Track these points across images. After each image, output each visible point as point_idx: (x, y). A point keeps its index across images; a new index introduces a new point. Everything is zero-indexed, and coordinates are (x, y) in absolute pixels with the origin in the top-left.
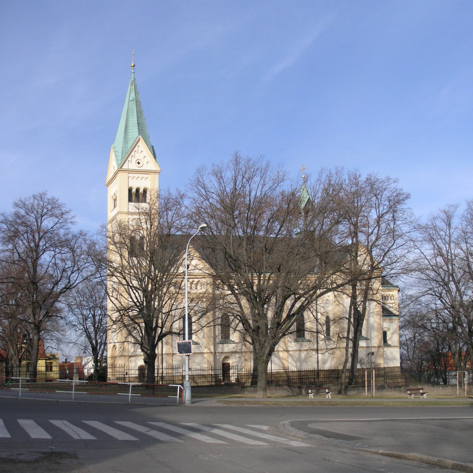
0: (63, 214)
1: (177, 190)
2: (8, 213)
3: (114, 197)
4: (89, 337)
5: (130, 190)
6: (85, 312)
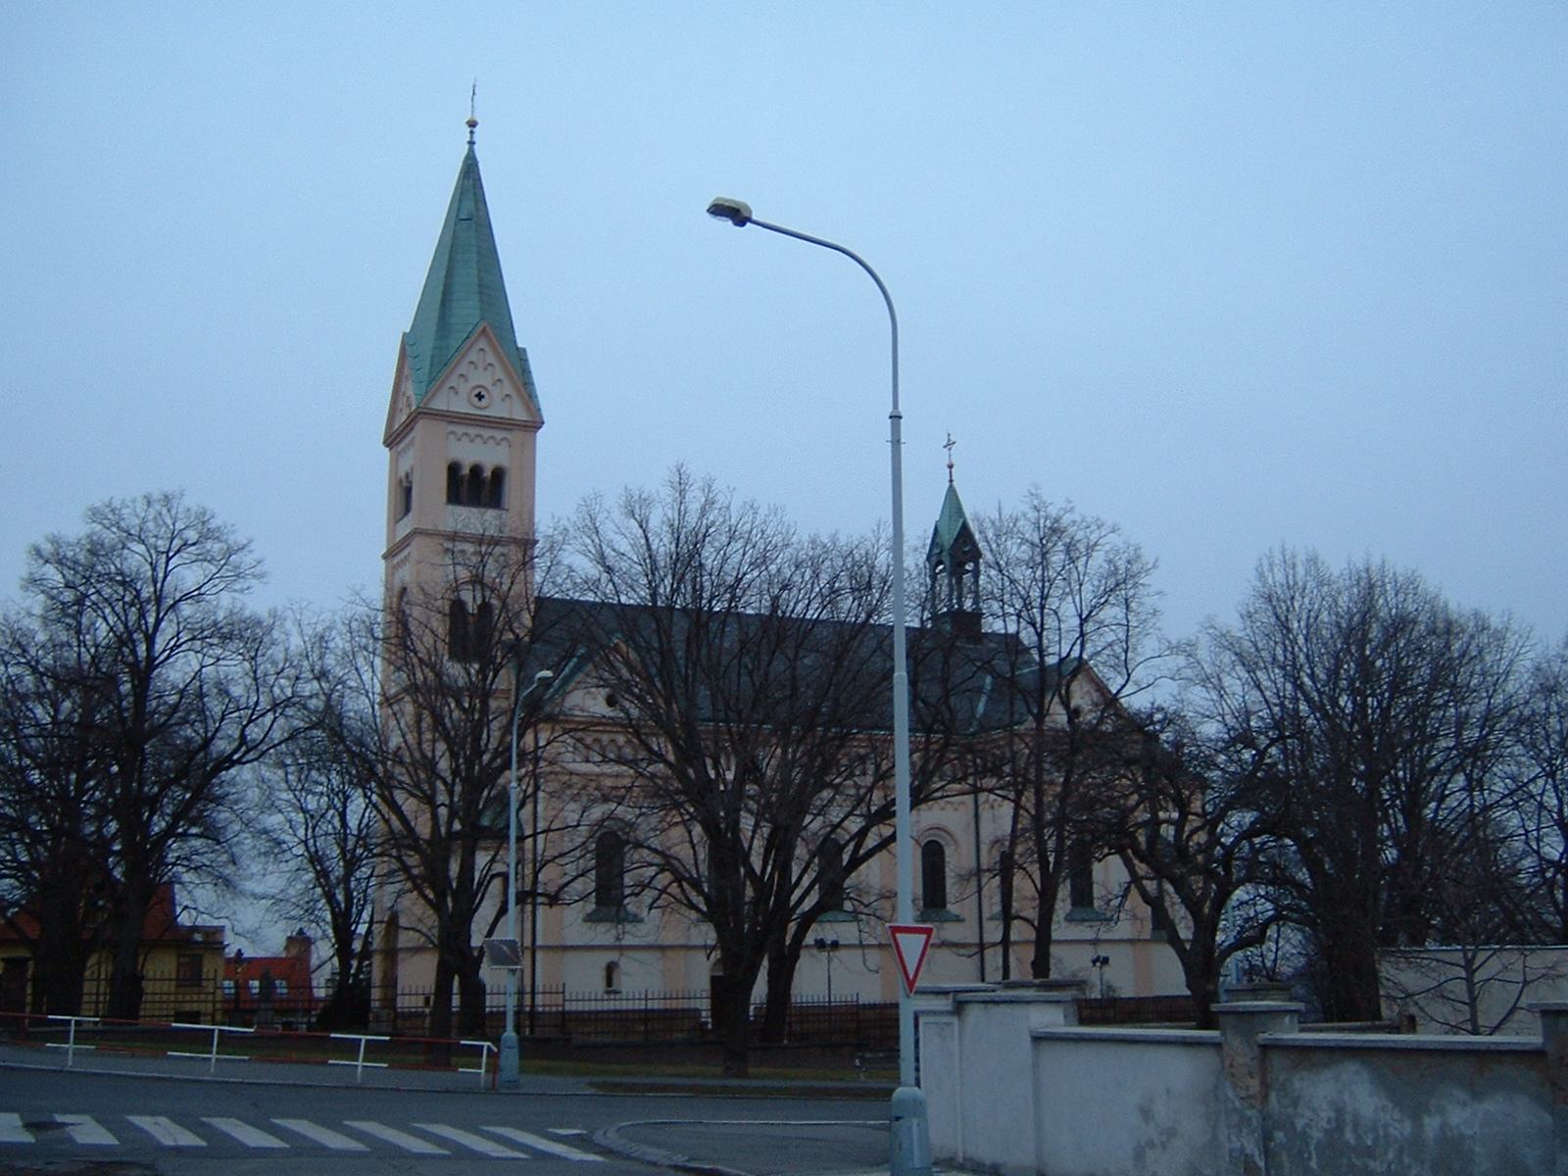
0: (229, 553)
1: (553, 517)
2: (73, 539)
3: (405, 484)
4: (323, 875)
5: (453, 469)
6: (312, 803)
